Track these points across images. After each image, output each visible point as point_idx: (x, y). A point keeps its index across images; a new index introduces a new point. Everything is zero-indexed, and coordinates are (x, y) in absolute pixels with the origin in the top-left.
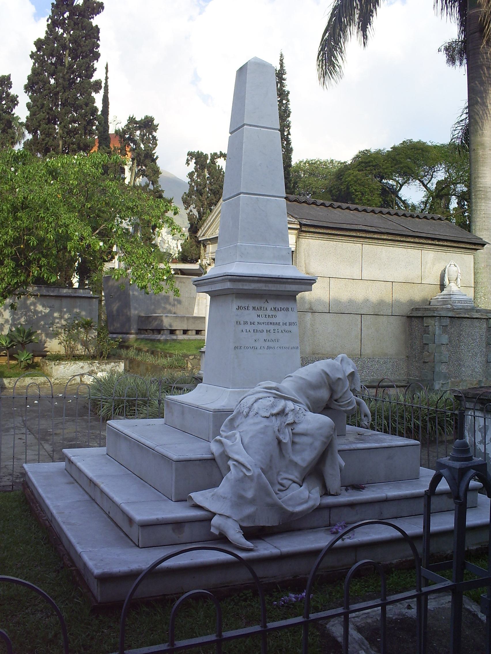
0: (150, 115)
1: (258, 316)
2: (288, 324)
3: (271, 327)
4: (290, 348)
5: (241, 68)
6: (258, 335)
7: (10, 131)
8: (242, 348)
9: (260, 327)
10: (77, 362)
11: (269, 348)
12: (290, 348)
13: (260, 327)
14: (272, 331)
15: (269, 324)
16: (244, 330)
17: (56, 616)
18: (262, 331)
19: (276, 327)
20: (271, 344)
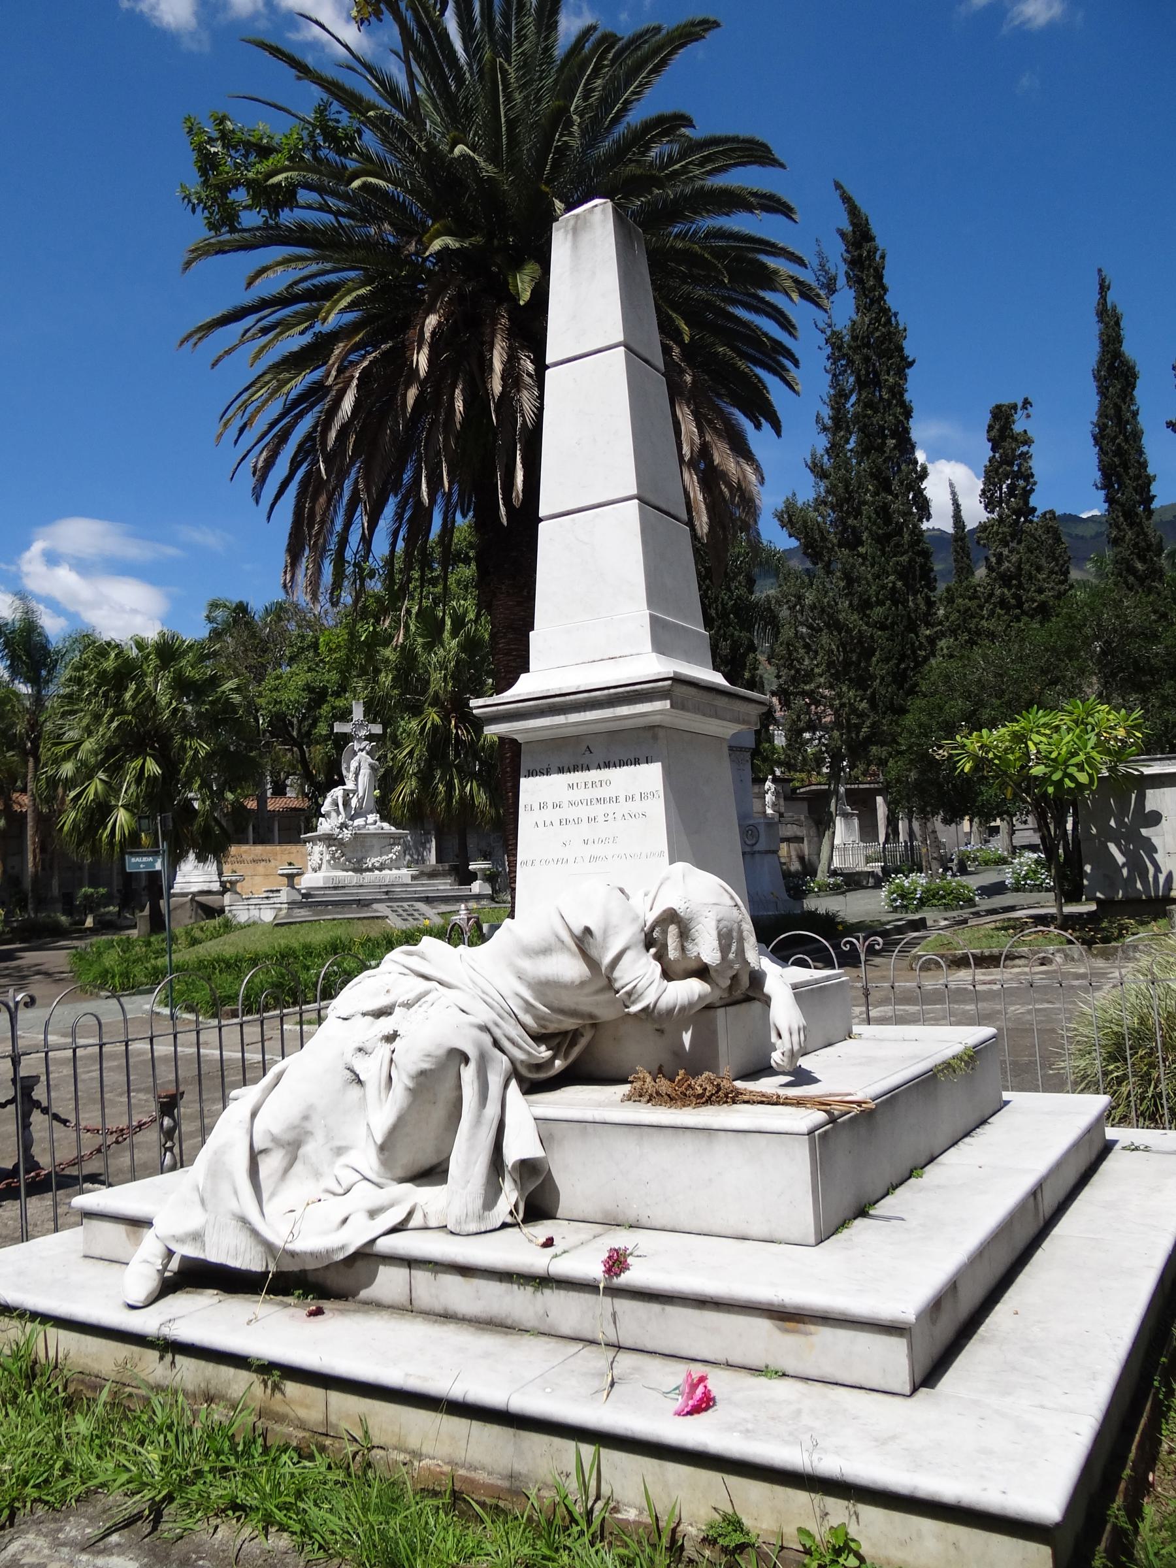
0: (245, 600)
1: (571, 786)
2: (637, 797)
3: (599, 810)
4: (644, 855)
5: (764, 147)
6: (569, 831)
7: (252, 158)
8: (537, 863)
9: (571, 813)
10: (447, 1469)
11: (592, 859)
12: (644, 855)
13: (571, 813)
14: (601, 819)
15: (594, 801)
16: (541, 824)
17: (120, 711)
18: (578, 821)
19: (609, 808)
20: (597, 849)
